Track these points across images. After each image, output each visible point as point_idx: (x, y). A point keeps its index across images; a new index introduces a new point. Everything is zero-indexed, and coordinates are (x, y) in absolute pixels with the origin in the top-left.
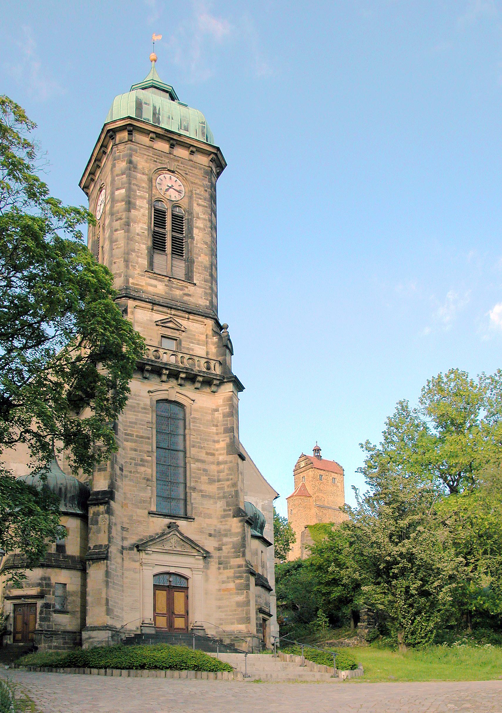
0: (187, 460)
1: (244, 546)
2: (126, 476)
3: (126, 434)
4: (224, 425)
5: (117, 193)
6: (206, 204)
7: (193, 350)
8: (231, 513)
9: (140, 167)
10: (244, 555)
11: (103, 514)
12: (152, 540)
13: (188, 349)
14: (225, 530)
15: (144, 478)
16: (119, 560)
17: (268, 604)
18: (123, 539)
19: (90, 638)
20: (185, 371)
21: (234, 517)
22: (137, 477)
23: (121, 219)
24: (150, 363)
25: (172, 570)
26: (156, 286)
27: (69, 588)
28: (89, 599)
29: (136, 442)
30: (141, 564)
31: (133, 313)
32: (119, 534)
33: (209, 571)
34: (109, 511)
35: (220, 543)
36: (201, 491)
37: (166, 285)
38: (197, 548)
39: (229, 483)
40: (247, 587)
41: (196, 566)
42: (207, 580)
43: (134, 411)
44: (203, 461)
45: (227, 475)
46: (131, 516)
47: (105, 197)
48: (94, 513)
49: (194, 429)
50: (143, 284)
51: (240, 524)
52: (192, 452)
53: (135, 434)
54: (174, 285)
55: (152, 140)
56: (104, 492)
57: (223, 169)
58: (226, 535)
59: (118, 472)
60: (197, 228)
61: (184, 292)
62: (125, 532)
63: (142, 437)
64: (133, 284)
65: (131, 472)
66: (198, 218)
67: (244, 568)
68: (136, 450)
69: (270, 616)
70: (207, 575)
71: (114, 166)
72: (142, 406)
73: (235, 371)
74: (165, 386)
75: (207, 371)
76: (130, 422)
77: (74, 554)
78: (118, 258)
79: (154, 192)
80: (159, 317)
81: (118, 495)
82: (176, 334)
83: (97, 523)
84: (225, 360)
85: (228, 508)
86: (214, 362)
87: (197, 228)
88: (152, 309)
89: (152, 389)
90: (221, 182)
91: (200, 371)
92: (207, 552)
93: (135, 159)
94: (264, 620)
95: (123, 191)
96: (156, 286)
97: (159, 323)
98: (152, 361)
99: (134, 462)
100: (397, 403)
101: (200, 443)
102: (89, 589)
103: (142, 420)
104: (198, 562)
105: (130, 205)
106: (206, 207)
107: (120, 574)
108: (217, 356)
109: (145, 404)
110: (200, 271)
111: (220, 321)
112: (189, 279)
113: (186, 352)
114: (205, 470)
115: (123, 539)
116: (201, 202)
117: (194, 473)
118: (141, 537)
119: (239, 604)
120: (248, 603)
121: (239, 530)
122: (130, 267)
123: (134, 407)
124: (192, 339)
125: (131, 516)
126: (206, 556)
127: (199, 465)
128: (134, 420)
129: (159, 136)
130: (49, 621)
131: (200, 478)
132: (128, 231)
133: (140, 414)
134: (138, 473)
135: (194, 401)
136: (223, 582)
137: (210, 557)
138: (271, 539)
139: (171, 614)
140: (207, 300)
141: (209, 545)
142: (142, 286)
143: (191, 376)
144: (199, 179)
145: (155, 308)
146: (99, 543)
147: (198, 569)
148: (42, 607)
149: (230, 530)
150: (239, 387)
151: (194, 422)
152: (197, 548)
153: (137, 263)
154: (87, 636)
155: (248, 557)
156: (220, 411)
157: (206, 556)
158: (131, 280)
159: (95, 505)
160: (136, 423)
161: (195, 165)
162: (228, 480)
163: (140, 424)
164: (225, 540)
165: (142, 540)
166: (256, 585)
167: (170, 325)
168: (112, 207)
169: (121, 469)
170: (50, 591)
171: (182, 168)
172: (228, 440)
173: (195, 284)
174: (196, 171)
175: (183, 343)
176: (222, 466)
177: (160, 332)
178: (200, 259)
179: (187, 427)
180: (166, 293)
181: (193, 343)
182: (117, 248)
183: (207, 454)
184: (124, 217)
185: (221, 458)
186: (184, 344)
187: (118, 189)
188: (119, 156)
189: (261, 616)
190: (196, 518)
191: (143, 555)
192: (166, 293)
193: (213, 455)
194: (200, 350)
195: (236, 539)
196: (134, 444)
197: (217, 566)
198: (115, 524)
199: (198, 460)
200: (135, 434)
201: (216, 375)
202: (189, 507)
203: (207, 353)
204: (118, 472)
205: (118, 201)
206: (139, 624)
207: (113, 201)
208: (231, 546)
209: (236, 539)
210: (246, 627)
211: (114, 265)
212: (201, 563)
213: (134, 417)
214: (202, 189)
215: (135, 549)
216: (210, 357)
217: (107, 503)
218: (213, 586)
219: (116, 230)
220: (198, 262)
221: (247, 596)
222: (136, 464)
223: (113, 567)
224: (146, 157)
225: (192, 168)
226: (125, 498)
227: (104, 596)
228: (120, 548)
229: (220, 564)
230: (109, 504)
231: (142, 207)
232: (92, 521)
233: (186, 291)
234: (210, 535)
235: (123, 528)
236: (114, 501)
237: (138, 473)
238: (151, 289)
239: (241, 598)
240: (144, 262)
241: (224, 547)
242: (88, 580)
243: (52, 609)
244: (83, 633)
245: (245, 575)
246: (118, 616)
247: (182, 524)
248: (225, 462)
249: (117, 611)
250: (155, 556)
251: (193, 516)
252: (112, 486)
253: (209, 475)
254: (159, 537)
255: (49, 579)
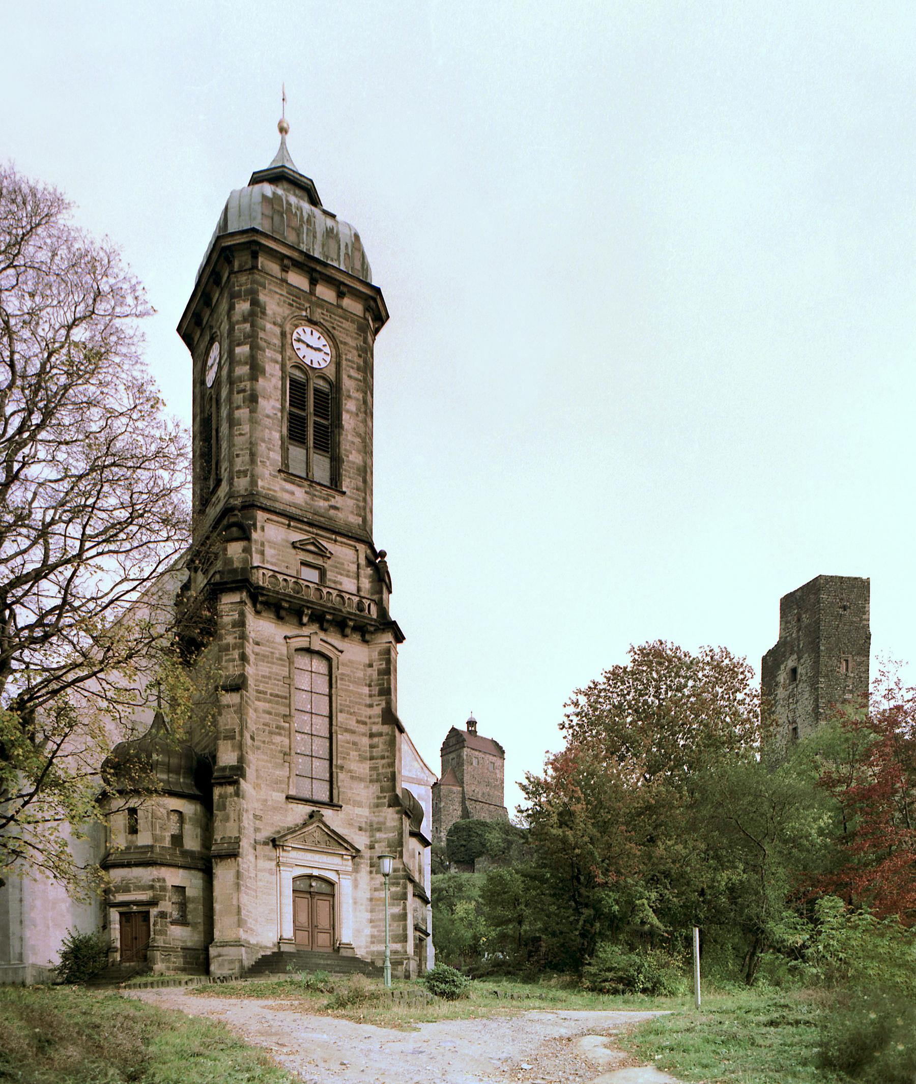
0: (334, 728)
1: (400, 844)
2: (258, 748)
3: (258, 692)
4: (380, 685)
5: (238, 350)
6: (359, 377)
7: (341, 584)
8: (386, 801)
9: (269, 312)
10: (401, 856)
11: (231, 797)
12: (292, 831)
13: (335, 582)
14: (378, 823)
15: (281, 752)
16: (252, 859)
17: (424, 920)
18: (257, 830)
19: (219, 956)
20: (331, 611)
21: (389, 806)
22: (271, 750)
23: (244, 391)
24: (287, 599)
25: (316, 873)
26: (293, 493)
27: (189, 893)
28: (217, 907)
29: (270, 702)
30: (278, 865)
31: (263, 529)
32: (251, 824)
33: (359, 875)
34: (237, 794)
35: (373, 839)
36: (350, 771)
37: (306, 492)
38: (346, 845)
39: (384, 761)
40: (404, 897)
41: (343, 868)
42: (356, 886)
43: (268, 662)
44: (353, 732)
45: (382, 751)
46: (266, 800)
47: (220, 353)
48: (220, 796)
49: (342, 689)
50: (277, 488)
51: (396, 816)
52: (339, 719)
53: (269, 691)
54: (317, 493)
55: (285, 269)
56: (232, 768)
57: (383, 324)
58: (379, 830)
59: (249, 742)
60: (348, 411)
61: (330, 503)
62: (257, 822)
63: (277, 696)
64: (263, 487)
65: (264, 742)
66: (349, 397)
67: (402, 873)
68: (270, 713)
69: (428, 935)
70: (356, 880)
71: (231, 308)
72: (277, 656)
73: (393, 615)
74: (306, 631)
75: (357, 612)
76: (263, 676)
77: (194, 849)
78: (242, 450)
79: (289, 352)
80: (297, 536)
81: (250, 772)
82: (319, 562)
83: (223, 807)
84: (381, 599)
85: (382, 795)
86: (369, 602)
87: (348, 411)
88: (289, 525)
89: (289, 634)
90: (383, 343)
91: (349, 613)
92: (358, 851)
93: (262, 297)
94: (421, 940)
95: (246, 348)
96: (293, 493)
97: (298, 545)
98: (291, 596)
99: (267, 728)
100: (579, 692)
101: (349, 707)
102: (216, 893)
103: (277, 674)
104: (345, 863)
105: (256, 371)
106: (360, 381)
107: (253, 875)
108: (372, 594)
109: (281, 654)
110: (352, 475)
111: (375, 546)
112: (335, 483)
113: (333, 585)
114: (355, 744)
115: (257, 830)
116: (353, 373)
117: (342, 746)
118: (278, 829)
119: (395, 917)
120: (404, 917)
121: (396, 823)
122: (259, 463)
123: (268, 657)
124: (340, 568)
125: (266, 800)
126: (356, 854)
127: (347, 736)
128: (267, 674)
129: (298, 265)
130: (166, 935)
131: (348, 754)
132: (253, 411)
133: (274, 667)
134: (274, 744)
135: (342, 652)
136: (376, 890)
137: (361, 857)
138: (429, 837)
139: (313, 928)
140: (360, 516)
141: (360, 841)
142: (275, 491)
143: (339, 619)
144: (352, 337)
145: (292, 524)
146: (228, 834)
147: (346, 873)
148: (156, 916)
149: (384, 823)
150: (399, 637)
151: (342, 679)
152: (346, 845)
153: (268, 458)
154: (216, 954)
155: (405, 859)
156: (375, 668)
157: (356, 854)
158: (260, 483)
159: (221, 784)
160: (270, 678)
161: (347, 315)
162: (383, 758)
163: (275, 679)
164: (378, 835)
165: (279, 832)
166: (414, 895)
167: (312, 548)
168: (231, 371)
169: (252, 738)
170: (165, 896)
171: (328, 318)
172: (384, 704)
173: (344, 493)
174: (347, 325)
175: (328, 573)
176: (376, 740)
177: (299, 557)
178: (351, 458)
179: (334, 686)
180: (306, 503)
181: (341, 574)
182: (241, 434)
183: (358, 722)
184: (248, 388)
185: (375, 729)
186: (330, 575)
187: (239, 345)
188: (240, 291)
189: (418, 933)
190: (344, 806)
191: (280, 852)
192: (306, 503)
193: (365, 723)
194: (349, 585)
195: (392, 835)
196: (267, 704)
197: (368, 869)
198: (247, 811)
199: (347, 730)
200: (269, 691)
201: (372, 619)
202: (335, 792)
203: (359, 589)
204: (249, 742)
205: (240, 363)
206: (276, 940)
207: (232, 359)
208: (384, 844)
209: (393, 835)
210: (403, 947)
211: (236, 459)
212: (348, 865)
213: (268, 670)
214: (355, 353)
215: (271, 844)
216: (362, 594)
217: (236, 783)
218: (364, 893)
219: (238, 408)
220: (348, 461)
221: (405, 908)
222: (271, 733)
223: (245, 866)
224: (277, 296)
225: (341, 320)
226: (257, 777)
227: (235, 902)
228: (253, 842)
229: (371, 866)
230: (239, 784)
231: (272, 375)
232: (218, 806)
233: (333, 502)
234: (360, 829)
235: (255, 816)
236: (245, 780)
237: (274, 744)
238: (286, 497)
239: (397, 910)
240: (276, 456)
241: (376, 845)
242: (215, 883)
243: (169, 920)
244: (210, 949)
245: (402, 881)
246: (252, 930)
247: (328, 814)
248: (380, 735)
249: (251, 923)
250: (294, 854)
251: (340, 803)
252: (241, 759)
253: (360, 750)
254: (300, 829)
255: (164, 880)
